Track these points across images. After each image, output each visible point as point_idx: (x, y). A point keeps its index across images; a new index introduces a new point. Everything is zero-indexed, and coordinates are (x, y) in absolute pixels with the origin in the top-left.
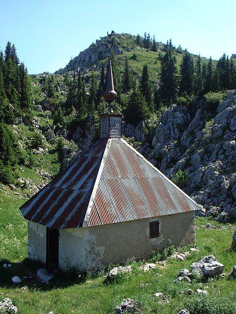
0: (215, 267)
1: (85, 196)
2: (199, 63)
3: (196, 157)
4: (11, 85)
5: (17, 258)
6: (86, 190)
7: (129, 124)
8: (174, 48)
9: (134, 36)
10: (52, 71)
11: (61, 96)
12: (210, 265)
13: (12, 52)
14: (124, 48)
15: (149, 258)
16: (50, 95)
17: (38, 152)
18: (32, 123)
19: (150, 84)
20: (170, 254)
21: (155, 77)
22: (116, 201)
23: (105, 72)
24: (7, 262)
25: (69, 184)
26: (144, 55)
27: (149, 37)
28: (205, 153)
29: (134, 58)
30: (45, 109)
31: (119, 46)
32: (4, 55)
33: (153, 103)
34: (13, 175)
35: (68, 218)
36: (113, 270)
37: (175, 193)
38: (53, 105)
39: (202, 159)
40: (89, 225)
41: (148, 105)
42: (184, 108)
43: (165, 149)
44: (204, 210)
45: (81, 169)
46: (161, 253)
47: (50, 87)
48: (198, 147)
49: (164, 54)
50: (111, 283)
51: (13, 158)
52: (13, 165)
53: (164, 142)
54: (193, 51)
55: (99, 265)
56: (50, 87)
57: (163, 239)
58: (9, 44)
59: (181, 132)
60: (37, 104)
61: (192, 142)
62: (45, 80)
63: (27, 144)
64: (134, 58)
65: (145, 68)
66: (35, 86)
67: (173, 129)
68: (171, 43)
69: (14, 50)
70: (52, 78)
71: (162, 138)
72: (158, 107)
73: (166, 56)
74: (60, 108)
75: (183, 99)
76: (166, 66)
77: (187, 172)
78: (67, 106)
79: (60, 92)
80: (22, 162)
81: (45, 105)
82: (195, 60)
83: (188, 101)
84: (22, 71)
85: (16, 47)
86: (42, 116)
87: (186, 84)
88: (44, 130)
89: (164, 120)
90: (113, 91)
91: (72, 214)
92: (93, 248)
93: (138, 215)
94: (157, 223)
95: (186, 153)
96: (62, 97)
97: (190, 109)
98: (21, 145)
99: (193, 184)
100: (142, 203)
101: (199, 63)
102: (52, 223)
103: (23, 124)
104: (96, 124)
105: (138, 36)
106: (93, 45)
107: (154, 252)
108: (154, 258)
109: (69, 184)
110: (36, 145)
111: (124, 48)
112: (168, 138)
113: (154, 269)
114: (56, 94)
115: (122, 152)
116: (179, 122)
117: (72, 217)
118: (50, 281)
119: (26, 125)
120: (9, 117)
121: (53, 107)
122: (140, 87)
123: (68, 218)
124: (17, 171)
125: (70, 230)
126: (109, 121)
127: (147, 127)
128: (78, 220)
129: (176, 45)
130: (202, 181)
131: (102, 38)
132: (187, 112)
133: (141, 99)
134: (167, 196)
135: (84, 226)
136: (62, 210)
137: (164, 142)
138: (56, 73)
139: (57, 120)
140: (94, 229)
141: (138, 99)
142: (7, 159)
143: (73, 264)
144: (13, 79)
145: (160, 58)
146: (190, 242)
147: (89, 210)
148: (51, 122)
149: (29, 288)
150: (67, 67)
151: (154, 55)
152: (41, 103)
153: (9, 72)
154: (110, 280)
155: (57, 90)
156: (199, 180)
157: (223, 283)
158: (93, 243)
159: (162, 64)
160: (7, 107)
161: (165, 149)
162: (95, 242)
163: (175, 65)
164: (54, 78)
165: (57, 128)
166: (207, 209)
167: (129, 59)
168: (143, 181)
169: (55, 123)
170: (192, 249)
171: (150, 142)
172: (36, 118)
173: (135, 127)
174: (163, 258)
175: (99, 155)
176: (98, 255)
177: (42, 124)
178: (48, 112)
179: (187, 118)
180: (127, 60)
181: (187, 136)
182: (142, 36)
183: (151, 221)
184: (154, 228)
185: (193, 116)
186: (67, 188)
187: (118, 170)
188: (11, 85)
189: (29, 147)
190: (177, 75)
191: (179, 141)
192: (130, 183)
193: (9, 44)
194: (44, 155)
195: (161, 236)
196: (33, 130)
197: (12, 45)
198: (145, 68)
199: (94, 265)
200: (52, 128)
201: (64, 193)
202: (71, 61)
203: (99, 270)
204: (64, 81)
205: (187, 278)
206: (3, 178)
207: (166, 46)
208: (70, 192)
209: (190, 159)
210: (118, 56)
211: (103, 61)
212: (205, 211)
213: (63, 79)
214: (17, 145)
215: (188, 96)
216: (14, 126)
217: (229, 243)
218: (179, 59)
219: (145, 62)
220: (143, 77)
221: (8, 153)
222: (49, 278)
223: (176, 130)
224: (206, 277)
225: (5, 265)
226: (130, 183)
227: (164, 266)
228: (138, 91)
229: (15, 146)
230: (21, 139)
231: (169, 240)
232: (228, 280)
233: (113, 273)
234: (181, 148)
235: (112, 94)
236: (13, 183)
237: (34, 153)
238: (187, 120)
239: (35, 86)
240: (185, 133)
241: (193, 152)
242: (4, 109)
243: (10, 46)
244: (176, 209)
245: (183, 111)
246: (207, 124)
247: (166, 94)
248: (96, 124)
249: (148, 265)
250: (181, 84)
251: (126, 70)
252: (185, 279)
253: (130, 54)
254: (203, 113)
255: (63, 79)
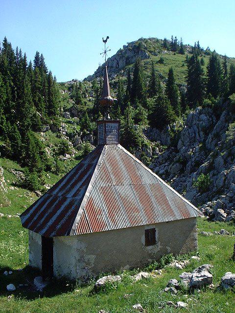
0: (202, 278)
1: (76, 203)
2: (224, 64)
3: (220, 160)
4: (38, 93)
5: (20, 265)
6: (78, 198)
7: (154, 129)
8: (202, 50)
9: (162, 40)
10: (81, 78)
11: (89, 102)
12: (198, 276)
13: (40, 62)
14: (151, 52)
15: (144, 267)
16: (78, 102)
17: (65, 158)
18: (59, 130)
19: (175, 87)
20: (167, 262)
21: (181, 80)
22: (109, 209)
23: (132, 77)
24: (8, 269)
25: (64, 191)
26: (170, 58)
27: (176, 40)
28: (228, 156)
29: (161, 61)
30: (73, 115)
31: (146, 51)
32: (33, 65)
33: (179, 106)
34: (39, 181)
35: (59, 226)
36: (100, 280)
37: (175, 199)
38: (81, 111)
39: (226, 162)
40: (77, 233)
41: (174, 109)
42: (210, 110)
43: (190, 152)
44: (225, 215)
45: (77, 176)
46: (159, 261)
47: (77, 94)
48: (221, 150)
49: (190, 56)
50: (96, 292)
51: (40, 165)
52: (39, 172)
53: (189, 146)
54: (221, 52)
55: (90, 274)
56: (77, 94)
57: (160, 247)
58: (37, 54)
59: (206, 134)
60: (65, 111)
61: (216, 145)
62: (73, 87)
63: (54, 150)
64: (161, 61)
65: (171, 71)
66: (63, 93)
67: (199, 132)
68: (198, 45)
69: (43, 59)
70: (80, 85)
71: (187, 142)
72: (183, 111)
73: (192, 58)
74: (87, 114)
75: (207, 101)
76: (192, 68)
77: (209, 176)
78: (93, 112)
79: (88, 99)
80: (48, 169)
81: (73, 112)
82: (222, 61)
83: (213, 102)
84: (49, 80)
85: (44, 56)
86: (69, 122)
87: (214, 85)
88: (70, 136)
89: (189, 123)
90: (110, 97)
91: (63, 221)
92: (83, 257)
93: (131, 222)
94: (154, 230)
95: (209, 157)
96: (90, 103)
97: (216, 111)
98: (48, 151)
99: (215, 188)
100: (137, 210)
101: (224, 64)
102: (44, 231)
103: (50, 131)
104: (122, 130)
105: (165, 40)
106: (120, 51)
107: (150, 260)
108: (150, 267)
109: (64, 191)
110: (63, 151)
111: (151, 52)
112: (193, 141)
113: (146, 279)
114: (83, 100)
115: (118, 157)
116: (204, 124)
117: (63, 225)
118: (44, 289)
119: (54, 132)
120: (37, 125)
121: (80, 113)
122: (166, 91)
123: (59, 226)
124: (43, 177)
125: (62, 238)
126: (105, 127)
127: (173, 131)
128: (66, 229)
129: (204, 46)
130: (224, 185)
131: (129, 44)
132: (212, 114)
133: (166, 102)
134: (166, 201)
135: (71, 234)
136: (54, 218)
137: (189, 146)
138: (85, 79)
139: (84, 126)
140: (82, 237)
141: (163, 103)
142: (33, 166)
143: (65, 272)
144: (39, 88)
145: (187, 61)
146: (192, 250)
147: (78, 218)
148: (78, 128)
149: (15, 296)
150: (96, 73)
151: (181, 58)
152: (70, 110)
153: (36, 81)
154: (98, 289)
155: (85, 97)
156: (221, 184)
157: (209, 295)
158: (83, 251)
159: (188, 66)
160: (35, 115)
161: (190, 152)
162: (85, 250)
163: (202, 67)
164: (83, 85)
165: (84, 133)
166: (228, 214)
167: (156, 63)
168: (139, 187)
169: (82, 130)
170: (193, 257)
171: (176, 146)
172: (63, 125)
173: (161, 132)
174: (160, 266)
175: (95, 162)
176: (88, 263)
177: (70, 131)
178: (76, 119)
179: (212, 120)
180: (153, 64)
181: (212, 138)
182: (169, 39)
183: (147, 228)
184: (150, 236)
185: (218, 117)
186: (62, 195)
187: (112, 177)
188: (38, 93)
189: (56, 154)
190: (204, 77)
191: (204, 145)
192: (125, 190)
193: (37, 54)
194: (71, 161)
195: (159, 244)
196: (60, 137)
197: (40, 55)
198: (171, 71)
199: (84, 274)
200: (79, 134)
201: (59, 201)
202: (99, 68)
203: (88, 279)
204: (92, 87)
205: (173, 288)
206: (29, 185)
207: (193, 48)
208: (65, 199)
209: (213, 162)
210: (145, 60)
211: (131, 66)
212: (225, 216)
213: (91, 85)
214: (43, 152)
215: (213, 98)
216: (42, 133)
217: (230, 252)
218: (207, 60)
219: (171, 65)
220: (169, 80)
221: (34, 160)
222: (43, 286)
223: (201, 133)
224: (194, 287)
225: (6, 272)
226: (125, 190)
227: (157, 275)
228: (164, 95)
229: (42, 153)
230: (48, 146)
231: (168, 248)
232: (90, 296)
233: (100, 283)
234: (205, 150)
235: (109, 101)
236: (39, 190)
237: (61, 160)
238: (213, 122)
239: (63, 93)
240: (210, 135)
241: (216, 155)
242: (31, 117)
243: (38, 56)
244: (173, 214)
245: (208, 113)
246: (230, 126)
247: (193, 97)
248: (122, 130)
249: (142, 273)
250: (209, 86)
251: (153, 74)
252: (171, 291)
253: (157, 58)
254: (228, 114)
255: (91, 85)
